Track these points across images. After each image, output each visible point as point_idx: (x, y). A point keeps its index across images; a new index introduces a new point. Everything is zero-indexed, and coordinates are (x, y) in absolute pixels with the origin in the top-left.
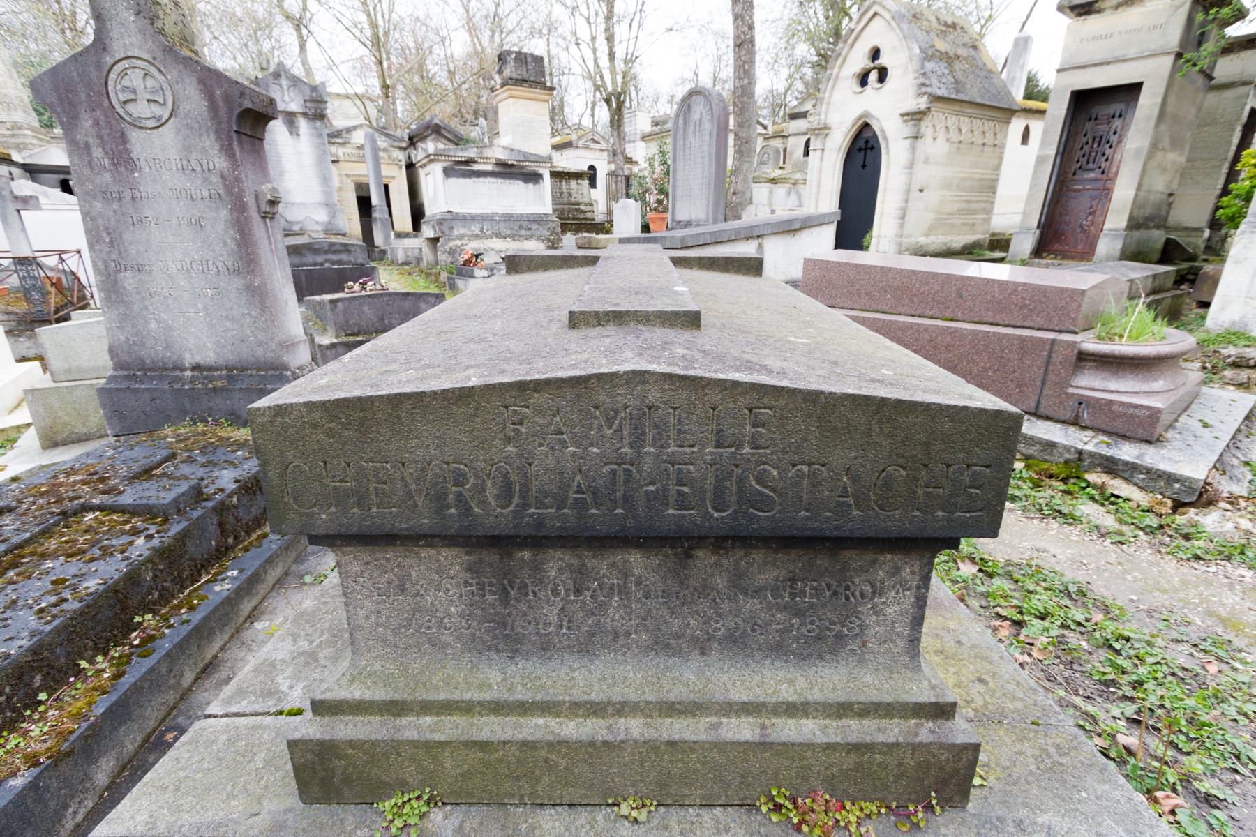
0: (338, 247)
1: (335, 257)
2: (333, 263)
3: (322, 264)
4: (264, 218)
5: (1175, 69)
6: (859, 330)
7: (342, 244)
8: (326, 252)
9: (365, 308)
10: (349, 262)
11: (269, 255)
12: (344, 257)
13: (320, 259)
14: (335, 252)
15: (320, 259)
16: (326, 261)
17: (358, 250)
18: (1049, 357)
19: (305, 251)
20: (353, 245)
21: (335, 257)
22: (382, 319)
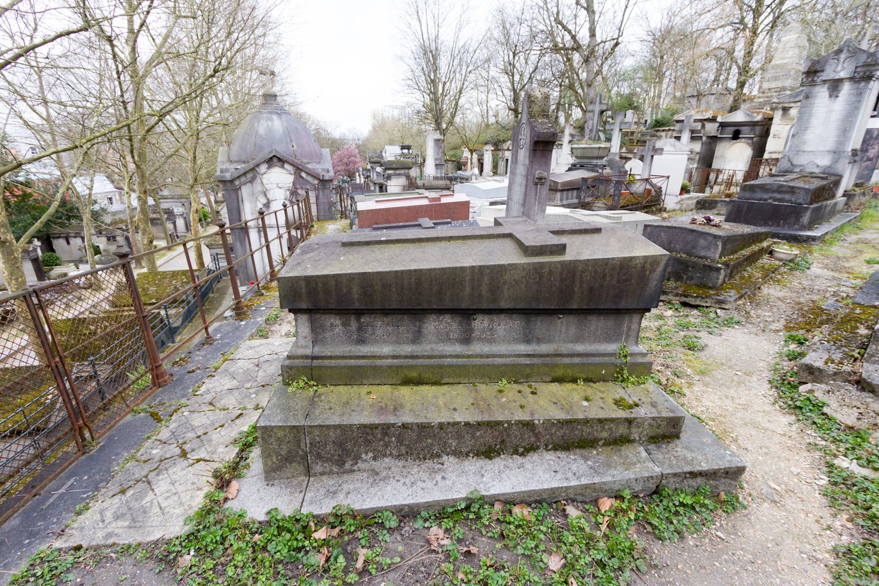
0: (785, 189)
1: (778, 196)
2: (775, 200)
3: (766, 200)
4: (536, 184)
5: (184, 273)
6: (457, 261)
7: (789, 187)
8: (774, 192)
9: (662, 234)
10: (790, 201)
11: (533, 200)
12: (787, 197)
13: (765, 196)
14: (780, 192)
15: (765, 196)
16: (770, 198)
17: (802, 192)
18: (153, 127)
19: (757, 189)
20: (799, 188)
21: (778, 196)
22: (670, 243)
